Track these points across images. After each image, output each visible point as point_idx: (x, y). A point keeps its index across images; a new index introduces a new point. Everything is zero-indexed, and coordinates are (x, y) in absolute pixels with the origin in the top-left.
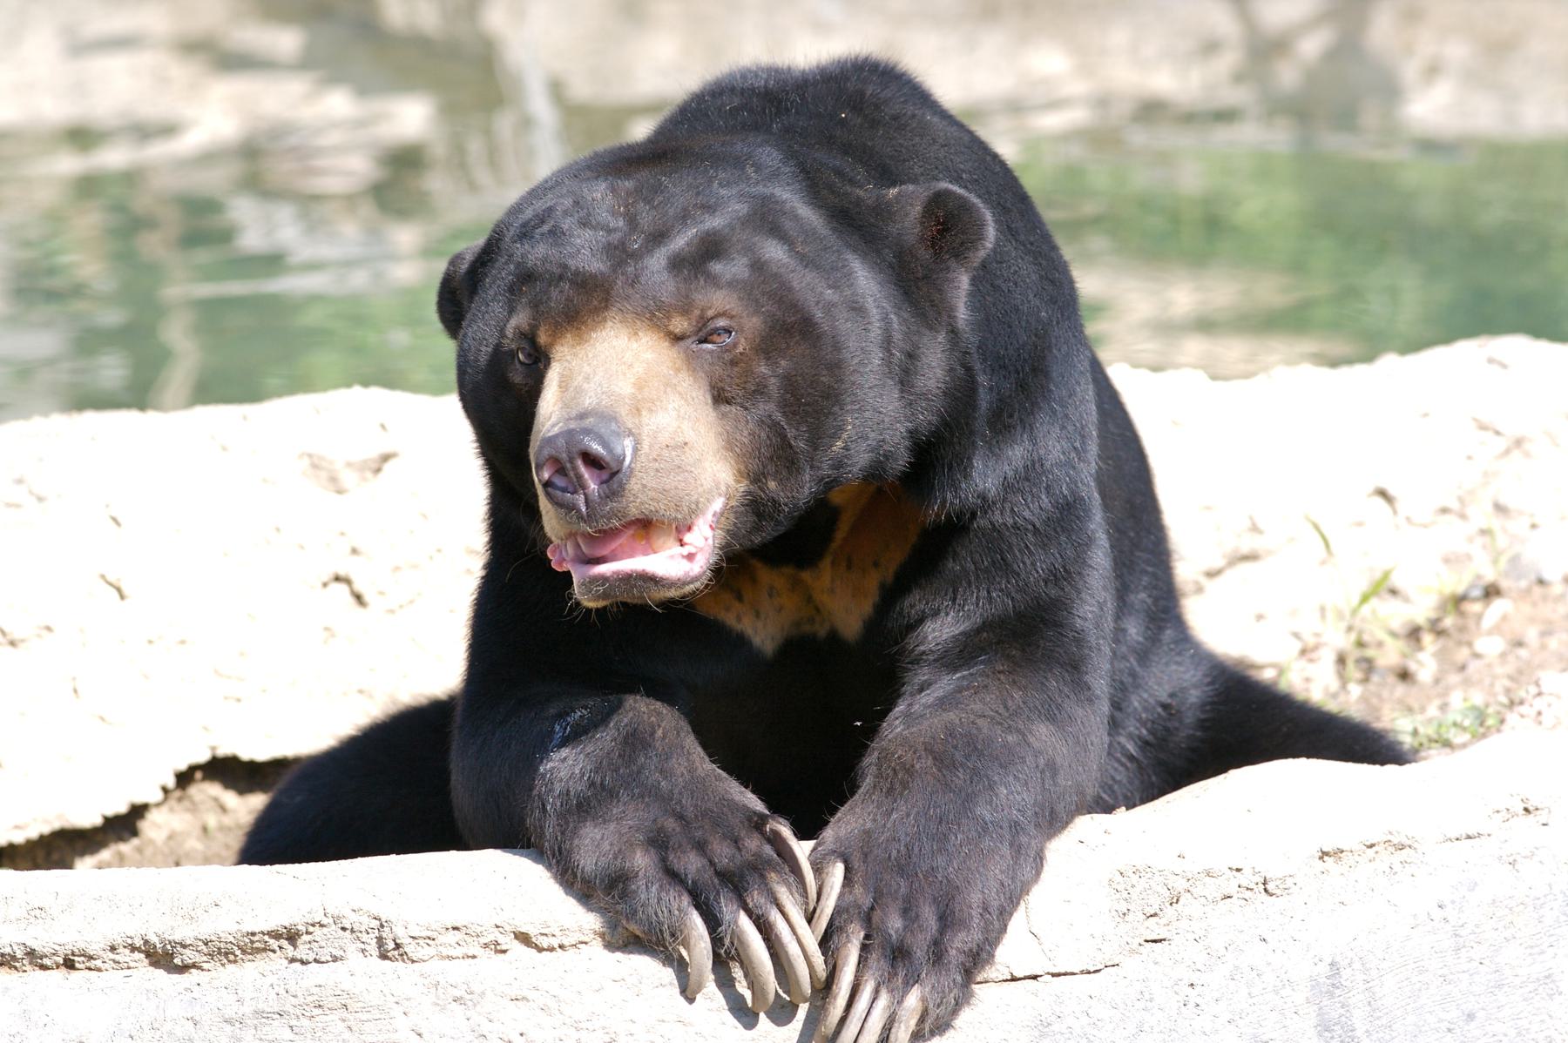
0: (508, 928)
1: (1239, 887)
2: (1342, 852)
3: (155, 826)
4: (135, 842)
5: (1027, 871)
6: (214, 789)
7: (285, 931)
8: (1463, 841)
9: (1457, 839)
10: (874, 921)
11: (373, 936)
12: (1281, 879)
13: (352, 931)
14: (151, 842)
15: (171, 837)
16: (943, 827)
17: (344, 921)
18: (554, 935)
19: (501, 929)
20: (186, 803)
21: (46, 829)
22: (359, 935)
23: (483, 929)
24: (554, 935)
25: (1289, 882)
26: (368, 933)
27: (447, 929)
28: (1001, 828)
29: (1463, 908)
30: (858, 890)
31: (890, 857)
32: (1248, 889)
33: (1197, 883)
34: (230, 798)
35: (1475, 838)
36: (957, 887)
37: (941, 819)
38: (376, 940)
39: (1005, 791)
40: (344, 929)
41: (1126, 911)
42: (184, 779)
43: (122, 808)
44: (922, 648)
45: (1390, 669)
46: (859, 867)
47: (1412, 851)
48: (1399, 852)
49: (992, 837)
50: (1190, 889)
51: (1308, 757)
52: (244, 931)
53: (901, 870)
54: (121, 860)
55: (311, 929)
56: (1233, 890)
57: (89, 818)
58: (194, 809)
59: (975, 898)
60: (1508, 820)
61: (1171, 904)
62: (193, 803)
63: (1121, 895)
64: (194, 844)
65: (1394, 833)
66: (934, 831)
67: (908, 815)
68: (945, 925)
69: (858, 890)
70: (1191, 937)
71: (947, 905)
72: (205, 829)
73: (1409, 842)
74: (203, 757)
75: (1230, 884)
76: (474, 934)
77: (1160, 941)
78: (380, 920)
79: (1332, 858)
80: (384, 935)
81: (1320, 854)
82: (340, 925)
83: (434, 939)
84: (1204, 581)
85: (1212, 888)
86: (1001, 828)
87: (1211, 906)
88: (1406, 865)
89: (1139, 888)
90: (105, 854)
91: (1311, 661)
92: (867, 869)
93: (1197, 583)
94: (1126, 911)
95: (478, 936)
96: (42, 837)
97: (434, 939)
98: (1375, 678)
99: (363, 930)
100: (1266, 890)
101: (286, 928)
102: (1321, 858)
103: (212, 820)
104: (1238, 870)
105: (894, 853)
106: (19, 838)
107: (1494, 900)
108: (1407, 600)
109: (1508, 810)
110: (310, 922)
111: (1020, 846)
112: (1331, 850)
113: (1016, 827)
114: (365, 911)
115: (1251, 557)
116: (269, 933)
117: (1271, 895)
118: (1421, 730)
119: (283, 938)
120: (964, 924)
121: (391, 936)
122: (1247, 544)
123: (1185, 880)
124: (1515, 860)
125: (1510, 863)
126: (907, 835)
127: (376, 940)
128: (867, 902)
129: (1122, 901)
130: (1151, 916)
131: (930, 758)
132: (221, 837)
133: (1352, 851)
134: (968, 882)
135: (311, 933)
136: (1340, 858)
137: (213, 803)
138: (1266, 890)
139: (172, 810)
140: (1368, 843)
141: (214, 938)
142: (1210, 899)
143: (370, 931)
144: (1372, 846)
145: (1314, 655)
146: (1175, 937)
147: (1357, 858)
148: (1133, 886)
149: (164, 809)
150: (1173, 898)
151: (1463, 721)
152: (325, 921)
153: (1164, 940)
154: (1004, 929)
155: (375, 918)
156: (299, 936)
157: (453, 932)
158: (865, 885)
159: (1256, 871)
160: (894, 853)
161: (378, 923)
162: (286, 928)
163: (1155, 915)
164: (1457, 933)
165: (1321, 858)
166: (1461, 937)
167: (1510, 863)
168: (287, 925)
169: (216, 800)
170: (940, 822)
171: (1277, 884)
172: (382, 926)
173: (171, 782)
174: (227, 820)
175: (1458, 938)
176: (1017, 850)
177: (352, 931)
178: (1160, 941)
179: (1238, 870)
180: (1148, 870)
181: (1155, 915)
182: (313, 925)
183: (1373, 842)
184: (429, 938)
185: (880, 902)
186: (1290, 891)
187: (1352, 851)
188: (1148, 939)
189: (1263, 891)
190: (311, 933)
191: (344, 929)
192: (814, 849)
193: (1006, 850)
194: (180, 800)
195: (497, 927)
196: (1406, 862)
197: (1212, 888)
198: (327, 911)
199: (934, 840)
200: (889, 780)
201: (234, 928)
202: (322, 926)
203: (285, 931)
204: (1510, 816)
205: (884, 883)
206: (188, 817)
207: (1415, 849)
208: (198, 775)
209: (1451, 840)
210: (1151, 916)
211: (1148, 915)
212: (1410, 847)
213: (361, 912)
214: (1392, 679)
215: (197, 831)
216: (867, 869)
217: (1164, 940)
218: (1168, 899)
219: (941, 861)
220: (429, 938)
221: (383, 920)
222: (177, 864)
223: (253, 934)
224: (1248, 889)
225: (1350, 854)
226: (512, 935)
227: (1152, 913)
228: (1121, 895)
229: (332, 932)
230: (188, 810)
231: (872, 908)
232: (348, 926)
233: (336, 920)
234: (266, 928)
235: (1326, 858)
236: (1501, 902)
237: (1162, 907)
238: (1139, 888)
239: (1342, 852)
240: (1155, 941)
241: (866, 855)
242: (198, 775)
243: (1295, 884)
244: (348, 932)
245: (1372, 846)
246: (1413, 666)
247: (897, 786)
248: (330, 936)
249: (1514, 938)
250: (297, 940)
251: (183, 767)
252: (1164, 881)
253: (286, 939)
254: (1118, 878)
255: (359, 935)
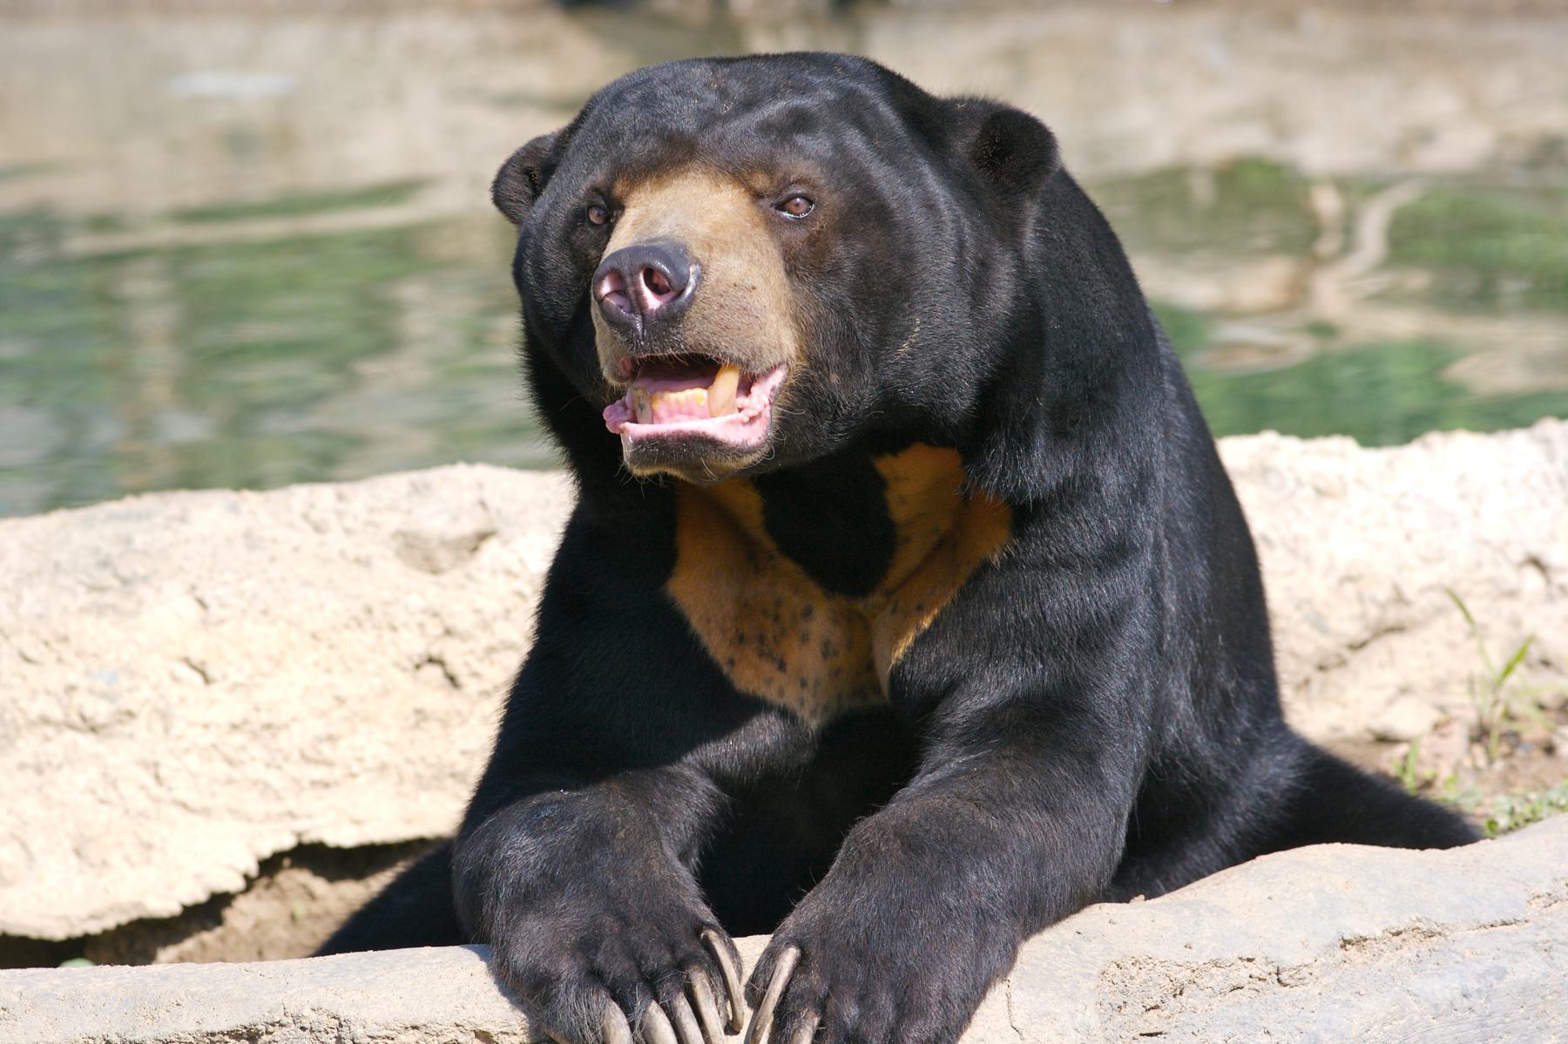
0: (468, 1027)
1: (1251, 977)
2: (1365, 940)
3: (239, 917)
4: (219, 931)
5: (994, 956)
6: (303, 877)
7: (245, 1031)
8: (1499, 928)
9: (1492, 926)
10: (828, 1010)
11: (332, 1036)
12: (1294, 969)
13: (312, 1031)
14: (234, 931)
15: (257, 925)
16: (904, 913)
17: (304, 1021)
18: (515, 1034)
19: (461, 1028)
20: (274, 890)
21: (124, 919)
22: (318, 1034)
23: (443, 1027)
24: (515, 1034)
25: (1305, 972)
26: (327, 1033)
27: (406, 1028)
28: (967, 914)
29: (1490, 997)
30: (815, 977)
31: (848, 943)
32: (1260, 979)
33: (1203, 974)
34: (319, 885)
35: (1511, 924)
36: (917, 974)
37: (903, 903)
38: (335, 1040)
39: (974, 878)
40: (303, 1029)
41: (1122, 1004)
42: (270, 866)
43: (201, 896)
44: (948, 720)
45: (1536, 743)
46: (816, 953)
47: (1443, 939)
48: (1428, 939)
49: (956, 924)
50: (1196, 980)
51: (1343, 842)
52: (204, 1031)
53: (860, 955)
54: (204, 955)
55: (271, 1029)
56: (1244, 981)
57: (165, 905)
58: (283, 896)
59: (935, 987)
60: (1550, 905)
61: (1174, 996)
62: (282, 891)
63: (1117, 988)
64: (280, 933)
65: (1424, 920)
66: (895, 916)
67: (868, 900)
68: (903, 1013)
69: (815, 977)
70: (1188, 1030)
71: (905, 993)
72: (293, 918)
73: (1439, 929)
74: (288, 842)
75: (1241, 974)
76: (433, 1033)
77: (1156, 1034)
78: (339, 1019)
79: (1355, 946)
80: (343, 1036)
81: (1342, 942)
82: (299, 1025)
83: (393, 1039)
84: (1347, 653)
85: (1218, 978)
86: (967, 914)
87: (1219, 997)
88: (1434, 952)
89: (1138, 981)
90: (189, 945)
91: (1443, 736)
92: (825, 955)
93: (1339, 656)
94: (1122, 1004)
95: (437, 1035)
96: (119, 928)
97: (393, 1039)
98: (1520, 753)
99: (322, 1029)
100: (1279, 981)
101: (245, 1028)
102: (1343, 947)
103: (300, 907)
104: (1250, 960)
105: (853, 939)
106: (95, 928)
107: (1524, 989)
108: (1560, 672)
109: (1550, 895)
110: (269, 1021)
111: (986, 934)
112: (1352, 938)
113: (983, 914)
114: (324, 1009)
115: (1397, 629)
116: (229, 1034)
117: (1285, 985)
118: (1518, 809)
119: (244, 1038)
120: (922, 1013)
121: (349, 1036)
122: (1393, 615)
123: (1189, 971)
124: (1550, 948)
125: (1546, 950)
126: (866, 919)
127: (335, 1040)
128: (823, 988)
129: (1118, 993)
130: (1152, 1008)
131: (898, 842)
132: (308, 924)
133: (1375, 940)
134: (927, 969)
135: (271, 1033)
136: (1363, 946)
137: (301, 891)
138: (1279, 981)
139: (259, 897)
140: (1394, 931)
141: (173, 1038)
142: (1216, 989)
143: (329, 1030)
144: (1398, 934)
145: (1444, 730)
146: (1174, 1031)
147: (1383, 947)
148: (1132, 978)
149: (252, 896)
150: (1176, 990)
151: (1559, 799)
152: (285, 1020)
153: (1161, 1033)
154: (967, 1018)
155: (334, 1017)
156: (260, 1036)
157: (412, 1031)
158: (822, 972)
159: (1270, 960)
160: (853, 939)
161: (337, 1022)
162: (245, 1028)
163: (1156, 1007)
164: (1484, 1022)
165: (1343, 947)
166: (1488, 1027)
167: (1546, 950)
168: (247, 1025)
169: (304, 886)
170: (901, 908)
171: (1291, 974)
172: (341, 1025)
173: (253, 869)
174: (316, 908)
175: (1485, 1028)
176: (983, 938)
177: (312, 1031)
178: (1156, 1034)
179: (1250, 960)
180: (1149, 961)
181: (1156, 1007)
182: (273, 1025)
183: (1399, 930)
184: (388, 1038)
185: (836, 990)
186: (1306, 981)
187: (1375, 940)
188: (1144, 1032)
189: (1276, 982)
190: (271, 1033)
191: (303, 1029)
192: (773, 938)
193: (970, 938)
194: (268, 887)
195: (458, 1026)
196: (1434, 950)
197: (1218, 978)
198: (287, 1010)
199: (893, 924)
200: (854, 863)
201: (193, 1028)
202: (282, 1026)
203: (245, 1031)
204: (1552, 901)
205: (840, 969)
206: (276, 904)
207: (1445, 936)
208: (287, 862)
209: (1485, 927)
210: (1152, 1008)
211: (1148, 1007)
212: (1440, 934)
213: (321, 1011)
214: (1538, 754)
215: (285, 919)
216: (825, 955)
217: (1161, 1033)
218: (1170, 991)
219: (901, 946)
220: (388, 1038)
221: (342, 1019)
222: (261, 955)
223: (213, 1034)
224: (1260, 979)
225: (1374, 942)
226: (473, 1034)
227: (1153, 1005)
228: (1117, 988)
229: (292, 1032)
230: (276, 897)
231: (828, 997)
232: (307, 1025)
233: (296, 1019)
234: (225, 1028)
235: (1348, 947)
236: (1532, 990)
237: (1164, 999)
238: (1138, 981)
239: (1365, 940)
240: (1150, 1035)
241: (824, 941)
242: (287, 862)
243: (1311, 974)
244: (307, 1031)
245: (1398, 934)
246: (1557, 740)
247: (861, 869)
248: (289, 1036)
249: (1548, 1027)
250: (257, 1040)
251: (266, 852)
252: (1167, 972)
253: (247, 1039)
254: (1113, 969)
255: (318, 1034)
